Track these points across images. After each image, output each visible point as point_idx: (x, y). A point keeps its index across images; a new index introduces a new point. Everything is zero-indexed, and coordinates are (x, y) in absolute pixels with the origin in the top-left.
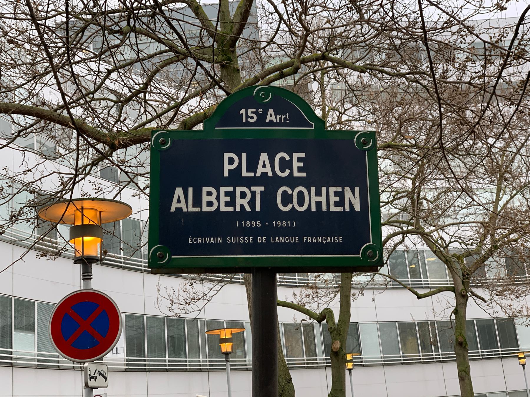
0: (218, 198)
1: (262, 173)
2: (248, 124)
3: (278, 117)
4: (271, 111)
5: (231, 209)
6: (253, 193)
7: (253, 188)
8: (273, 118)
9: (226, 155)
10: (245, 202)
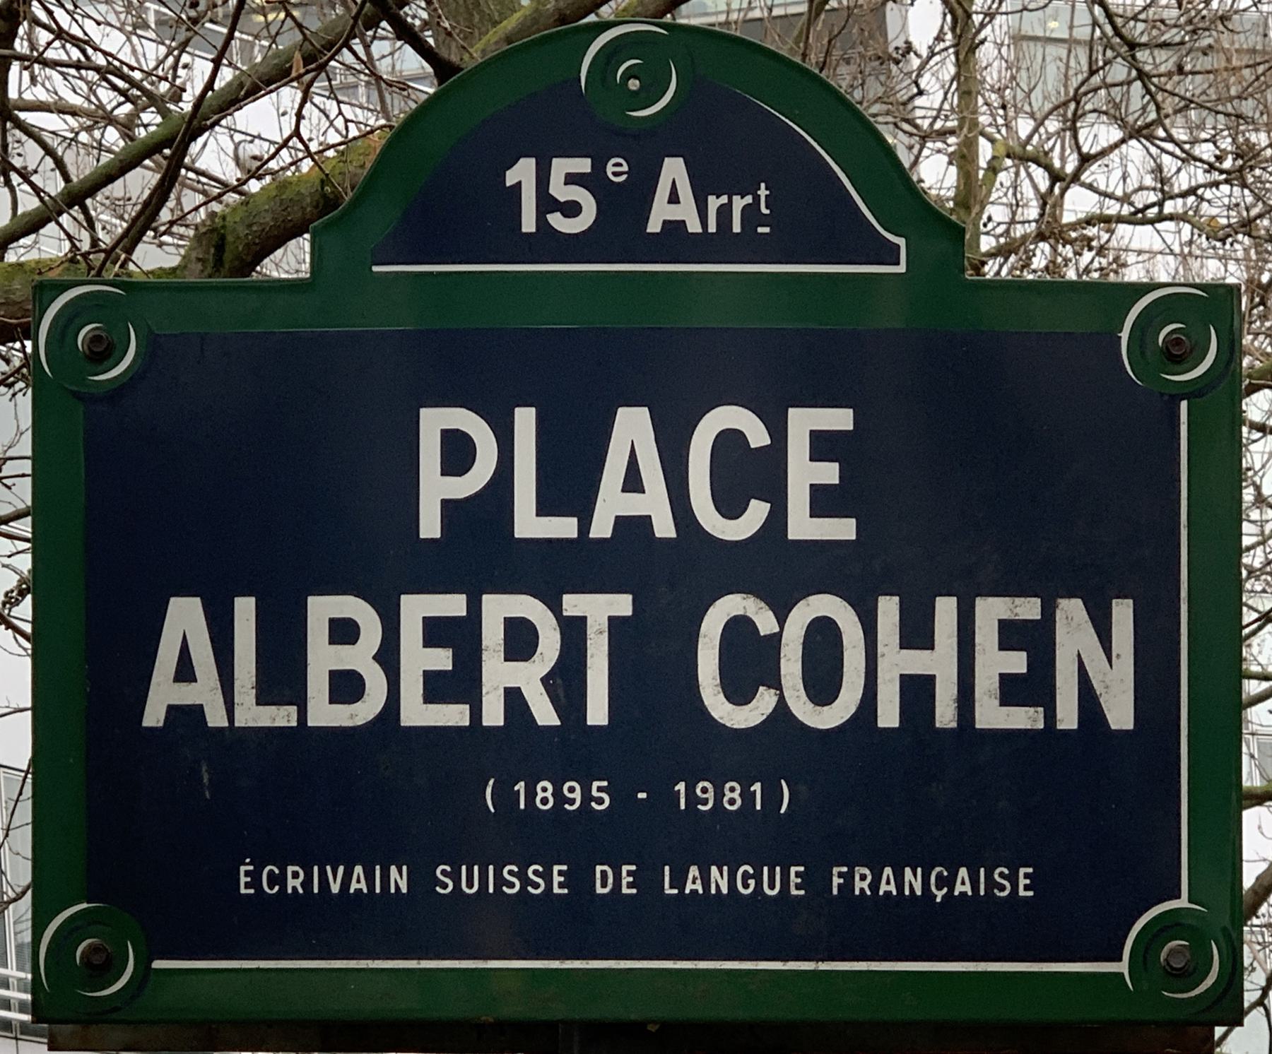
0: (388, 657)
2: (549, 244)
3: (714, 203)
4: (674, 170)
5: (454, 715)
6: (573, 630)
7: (573, 604)
8: (686, 212)
9: (434, 421)
10: (530, 677)
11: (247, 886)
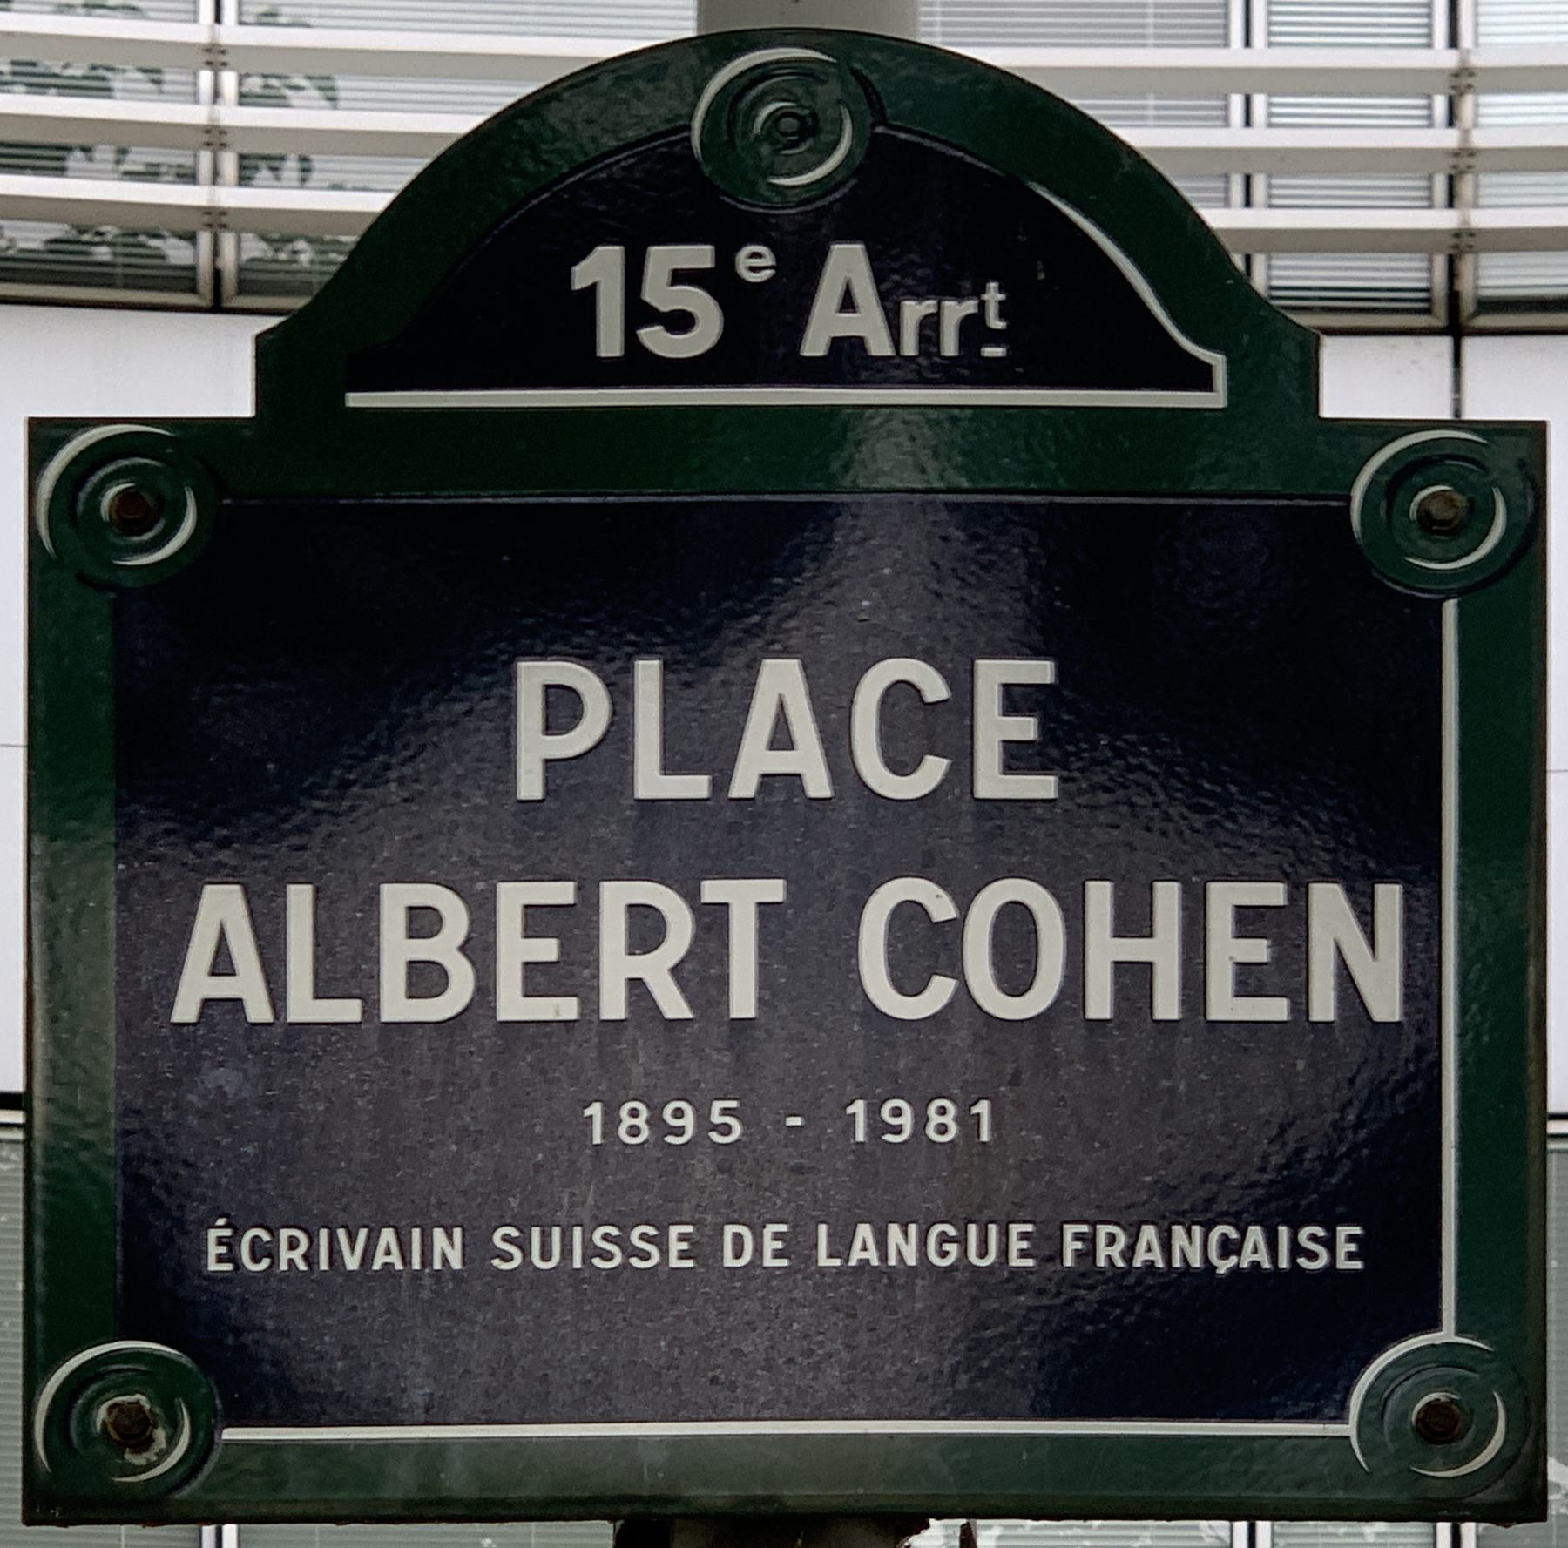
0: (480, 948)
1: (767, 780)
4: (847, 263)
7: (713, 890)
10: (656, 969)
11: (220, 1259)
